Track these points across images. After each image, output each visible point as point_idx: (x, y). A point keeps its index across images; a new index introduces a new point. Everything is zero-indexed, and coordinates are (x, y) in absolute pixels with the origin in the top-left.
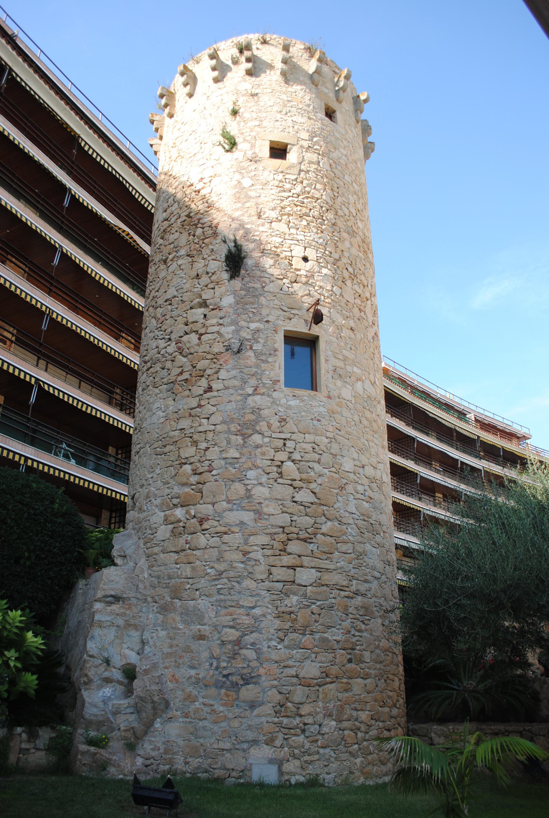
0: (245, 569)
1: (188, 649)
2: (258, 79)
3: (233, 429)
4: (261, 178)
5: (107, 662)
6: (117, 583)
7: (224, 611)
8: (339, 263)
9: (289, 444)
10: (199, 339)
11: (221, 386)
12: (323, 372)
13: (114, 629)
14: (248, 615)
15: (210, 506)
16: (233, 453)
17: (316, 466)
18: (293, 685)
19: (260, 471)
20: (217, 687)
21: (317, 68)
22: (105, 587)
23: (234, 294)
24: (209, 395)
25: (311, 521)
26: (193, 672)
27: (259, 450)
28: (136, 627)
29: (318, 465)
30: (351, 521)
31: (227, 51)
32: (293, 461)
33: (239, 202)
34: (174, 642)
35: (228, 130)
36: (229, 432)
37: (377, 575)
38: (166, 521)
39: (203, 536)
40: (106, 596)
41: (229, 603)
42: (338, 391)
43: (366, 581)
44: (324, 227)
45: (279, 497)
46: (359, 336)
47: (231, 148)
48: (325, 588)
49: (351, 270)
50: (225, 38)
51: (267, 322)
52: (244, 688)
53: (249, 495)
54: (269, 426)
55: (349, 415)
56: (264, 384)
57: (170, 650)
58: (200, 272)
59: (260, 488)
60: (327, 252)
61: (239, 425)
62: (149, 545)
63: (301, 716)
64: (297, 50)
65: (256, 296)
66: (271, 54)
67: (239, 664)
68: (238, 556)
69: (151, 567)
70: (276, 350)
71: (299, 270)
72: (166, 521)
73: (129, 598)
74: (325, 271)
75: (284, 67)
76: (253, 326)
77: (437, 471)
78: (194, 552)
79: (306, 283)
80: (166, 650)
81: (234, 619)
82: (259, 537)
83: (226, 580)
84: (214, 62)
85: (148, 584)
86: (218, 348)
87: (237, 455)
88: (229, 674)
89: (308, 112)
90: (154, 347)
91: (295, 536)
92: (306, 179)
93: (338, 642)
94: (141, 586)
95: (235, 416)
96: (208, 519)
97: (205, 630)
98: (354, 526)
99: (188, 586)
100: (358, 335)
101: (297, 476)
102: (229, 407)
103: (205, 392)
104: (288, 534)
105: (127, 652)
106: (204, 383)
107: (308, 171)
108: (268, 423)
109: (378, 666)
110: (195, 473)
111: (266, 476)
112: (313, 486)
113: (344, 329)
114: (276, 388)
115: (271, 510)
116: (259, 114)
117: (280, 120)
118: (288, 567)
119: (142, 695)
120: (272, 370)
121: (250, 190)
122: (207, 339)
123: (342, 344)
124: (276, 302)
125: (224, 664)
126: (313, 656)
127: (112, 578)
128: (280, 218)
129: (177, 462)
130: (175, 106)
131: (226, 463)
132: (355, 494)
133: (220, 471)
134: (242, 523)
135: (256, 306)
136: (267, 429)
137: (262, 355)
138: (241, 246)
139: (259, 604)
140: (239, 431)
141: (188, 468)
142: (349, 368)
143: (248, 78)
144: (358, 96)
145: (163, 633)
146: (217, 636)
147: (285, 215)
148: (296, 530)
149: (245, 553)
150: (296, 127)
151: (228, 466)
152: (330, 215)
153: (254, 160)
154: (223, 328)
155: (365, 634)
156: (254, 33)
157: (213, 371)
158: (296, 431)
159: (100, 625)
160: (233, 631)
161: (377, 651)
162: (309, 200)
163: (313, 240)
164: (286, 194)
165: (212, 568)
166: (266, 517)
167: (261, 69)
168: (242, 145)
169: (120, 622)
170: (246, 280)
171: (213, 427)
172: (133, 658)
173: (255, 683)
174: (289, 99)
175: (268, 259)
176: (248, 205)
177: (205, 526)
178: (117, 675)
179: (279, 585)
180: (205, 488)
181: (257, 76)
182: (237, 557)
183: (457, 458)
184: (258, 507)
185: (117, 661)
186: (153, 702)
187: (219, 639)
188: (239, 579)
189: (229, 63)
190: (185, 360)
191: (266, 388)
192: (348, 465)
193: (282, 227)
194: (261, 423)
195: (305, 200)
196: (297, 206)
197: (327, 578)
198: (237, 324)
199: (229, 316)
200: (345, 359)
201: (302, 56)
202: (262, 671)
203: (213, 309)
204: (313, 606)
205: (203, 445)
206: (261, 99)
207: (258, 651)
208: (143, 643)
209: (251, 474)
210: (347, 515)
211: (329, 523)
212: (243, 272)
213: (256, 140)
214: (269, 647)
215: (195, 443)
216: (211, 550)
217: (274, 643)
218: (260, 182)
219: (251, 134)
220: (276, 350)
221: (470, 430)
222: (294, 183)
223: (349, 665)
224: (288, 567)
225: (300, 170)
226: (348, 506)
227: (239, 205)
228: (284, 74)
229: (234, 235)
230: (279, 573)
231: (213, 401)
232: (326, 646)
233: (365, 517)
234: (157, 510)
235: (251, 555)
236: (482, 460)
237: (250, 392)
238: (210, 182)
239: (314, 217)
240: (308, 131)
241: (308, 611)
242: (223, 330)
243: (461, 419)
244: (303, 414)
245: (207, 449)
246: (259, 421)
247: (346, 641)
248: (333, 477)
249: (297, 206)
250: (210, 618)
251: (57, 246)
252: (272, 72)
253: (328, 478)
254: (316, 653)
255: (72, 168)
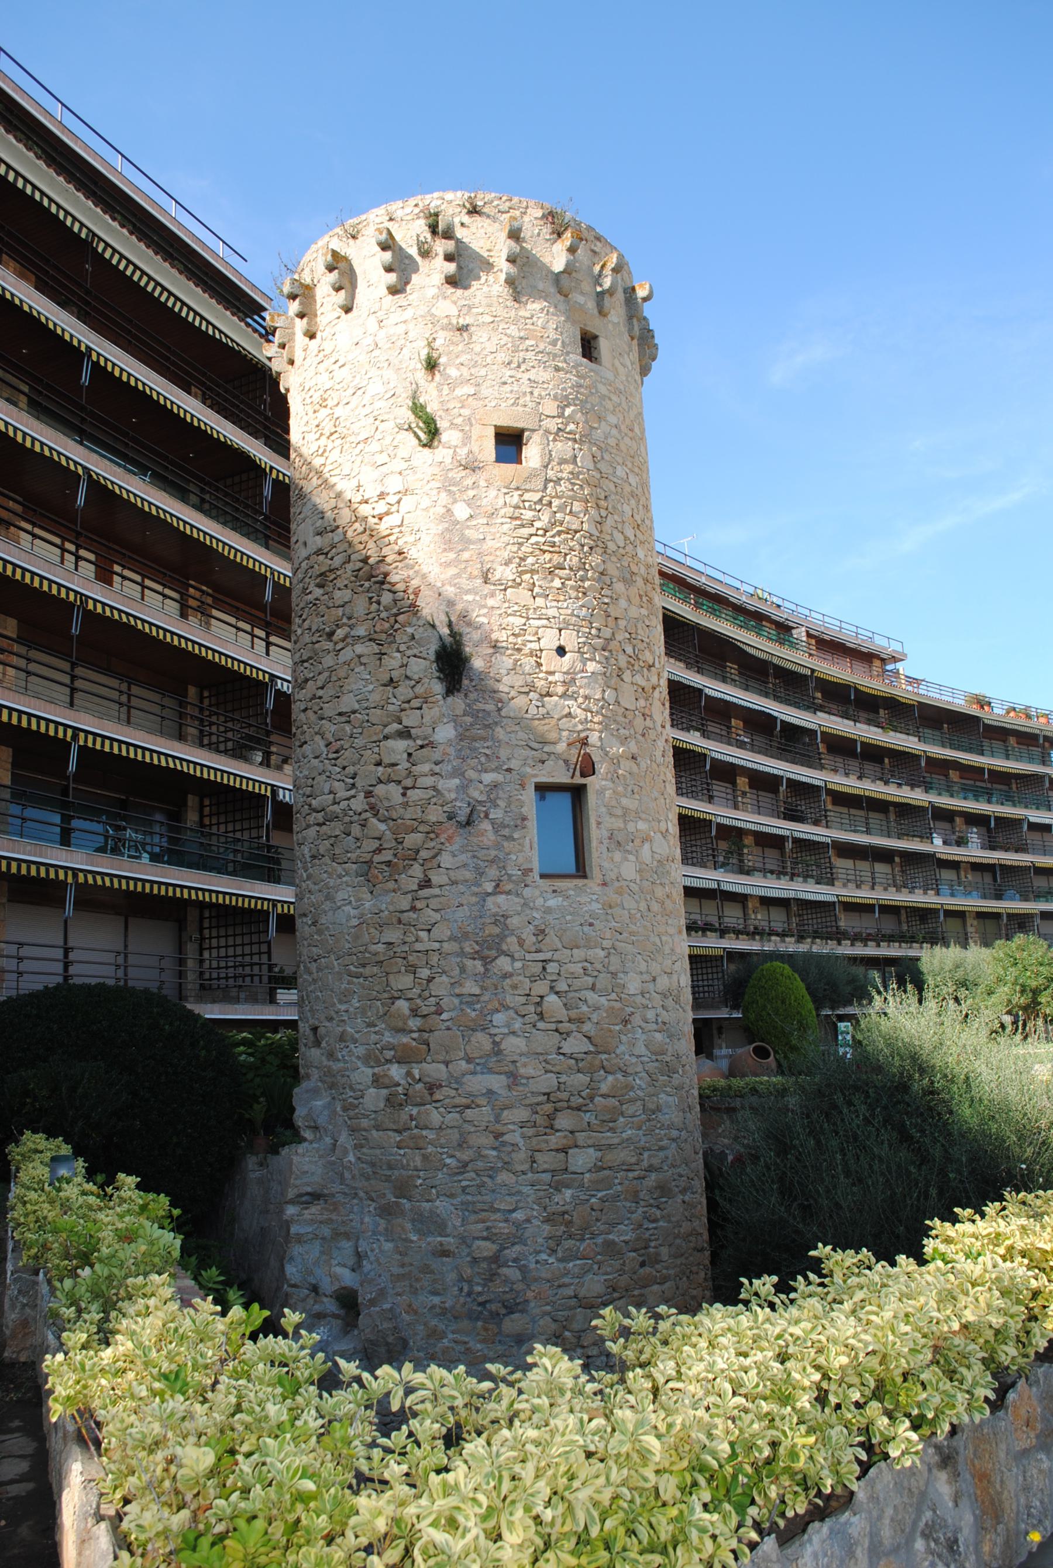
0: (498, 1157)
1: (426, 1269)
2: (467, 293)
3: (468, 949)
4: (484, 502)
5: (315, 1289)
6: (313, 1174)
7: (473, 1218)
8: (614, 645)
9: (552, 968)
10: (404, 795)
11: (444, 880)
12: (594, 843)
13: (318, 1242)
14: (506, 1221)
15: (442, 1067)
16: (471, 987)
17: (590, 996)
18: (571, 1308)
19: (511, 1012)
20: (470, 1318)
21: (568, 265)
22: (298, 1182)
23: (455, 721)
24: (426, 892)
25: (583, 1079)
26: (436, 1300)
27: (508, 980)
28: (347, 1236)
29: (591, 993)
30: (639, 1068)
31: (410, 233)
32: (557, 993)
33: (451, 550)
34: (407, 1260)
35: (422, 400)
36: (462, 953)
37: (674, 1133)
38: (377, 1081)
39: (435, 1112)
40: (301, 1195)
41: (479, 1206)
42: (616, 870)
43: (661, 1149)
44: (587, 584)
45: (539, 1050)
46: (644, 763)
47: (432, 440)
48: (607, 1172)
49: (629, 650)
50: (404, 194)
51: (509, 770)
52: (507, 1318)
53: (497, 1050)
54: (521, 943)
55: (633, 905)
56: (510, 876)
57: (401, 1271)
58: (395, 674)
59: (513, 1040)
60: (594, 631)
61: (477, 943)
62: (351, 1113)
63: (583, 1347)
64: (532, 222)
65: (488, 726)
66: (486, 238)
67: (499, 1288)
68: (486, 1140)
69: (358, 1147)
70: (524, 819)
71: (552, 673)
72: (377, 1081)
73: (333, 1195)
74: (591, 667)
75: (513, 270)
76: (488, 778)
77: (741, 745)
78: (424, 1133)
79: (564, 696)
80: (396, 1270)
81: (488, 1228)
82: (515, 1111)
83: (473, 1175)
84: (388, 256)
85: (356, 1172)
86: (435, 814)
87: (477, 991)
88: (486, 1302)
89: (555, 356)
90: (326, 791)
91: (565, 1104)
92: (557, 497)
93: (626, 1242)
94: (347, 1175)
95: (469, 929)
96: (441, 1086)
97: (449, 1243)
98: (644, 1074)
99: (420, 1181)
100: (643, 765)
101: (563, 1014)
102: (461, 914)
103: (421, 887)
104: (553, 1105)
105: (339, 1270)
106: (417, 870)
107: (560, 479)
108: (519, 938)
109: (678, 1261)
110: (415, 1012)
111: (520, 1020)
112: (587, 1027)
113: (623, 762)
114: (528, 882)
115: (531, 1071)
116: (473, 371)
117: (510, 380)
118: (557, 1150)
119: (373, 1338)
120: (521, 851)
121: (468, 527)
122: (416, 798)
123: (620, 789)
124: (521, 735)
125: (479, 1289)
126: (596, 1267)
127: (306, 1168)
128: (518, 580)
129: (386, 995)
130: (316, 316)
131: (461, 1003)
132: (644, 1025)
133: (453, 1014)
134: (490, 1092)
135: (489, 744)
136: (518, 948)
137: (505, 827)
138: (461, 635)
139: (521, 1205)
140: (477, 952)
141: (403, 1005)
142: (631, 827)
143: (450, 290)
144: (633, 289)
145: (388, 1246)
146: (467, 1250)
147: (526, 572)
148: (564, 1096)
149: (498, 1135)
150: (536, 394)
151: (464, 1007)
152: (595, 559)
153: (471, 466)
154: (442, 781)
155: (661, 1223)
156: (455, 190)
157: (431, 853)
158: (560, 946)
159: (300, 1239)
160: (487, 1244)
161: (678, 1241)
162: (563, 536)
163: (572, 615)
164: (525, 532)
165: (452, 1156)
166: (524, 1081)
167: (471, 271)
168: (448, 436)
169: (326, 1231)
170: (473, 696)
171: (437, 945)
172: (348, 1278)
173: (522, 1311)
174: (522, 334)
175: (505, 658)
176: (466, 555)
177: (437, 1096)
178: (330, 1305)
179: (546, 1177)
180: (433, 1039)
181: (466, 287)
182: (486, 1141)
183: (781, 773)
184: (512, 1068)
185: (328, 1286)
186: (387, 1344)
187: (468, 1255)
188: (492, 1172)
189: (413, 251)
190: (382, 827)
191: (513, 882)
192: (633, 985)
193: (522, 595)
194: (509, 940)
195: (557, 539)
196: (544, 552)
197: (611, 1158)
198: (463, 774)
199: (449, 761)
200: (626, 811)
201: (539, 235)
202: (530, 1294)
203: (422, 747)
204: (593, 1200)
205: (425, 973)
206: (474, 338)
207: (523, 1269)
208: (359, 1256)
209: (499, 1018)
210: (634, 1060)
211: (610, 1078)
212: (465, 682)
213: (471, 425)
214: (537, 1262)
215: (412, 969)
216: (449, 1131)
217: (544, 1256)
218: (483, 510)
219: (462, 411)
220: (524, 819)
221: (800, 658)
222: (538, 507)
223: (641, 1270)
224: (557, 1150)
225: (547, 481)
226: (634, 1048)
227: (452, 555)
228: (510, 282)
229: (447, 613)
230: (545, 1160)
231: (434, 903)
232: (611, 1249)
233: (658, 1052)
234: (359, 1064)
235: (506, 1138)
236: (819, 714)
237: (490, 890)
238: (399, 502)
239: (571, 569)
240: (555, 398)
241: (587, 1207)
242: (442, 784)
243: (781, 642)
244: (568, 918)
245: (430, 980)
246: (506, 936)
247: (638, 1239)
248: (613, 1008)
249: (544, 552)
250: (455, 1227)
251: (80, 471)
252: (491, 278)
253: (607, 1011)
254: (599, 1263)
255: (88, 303)
